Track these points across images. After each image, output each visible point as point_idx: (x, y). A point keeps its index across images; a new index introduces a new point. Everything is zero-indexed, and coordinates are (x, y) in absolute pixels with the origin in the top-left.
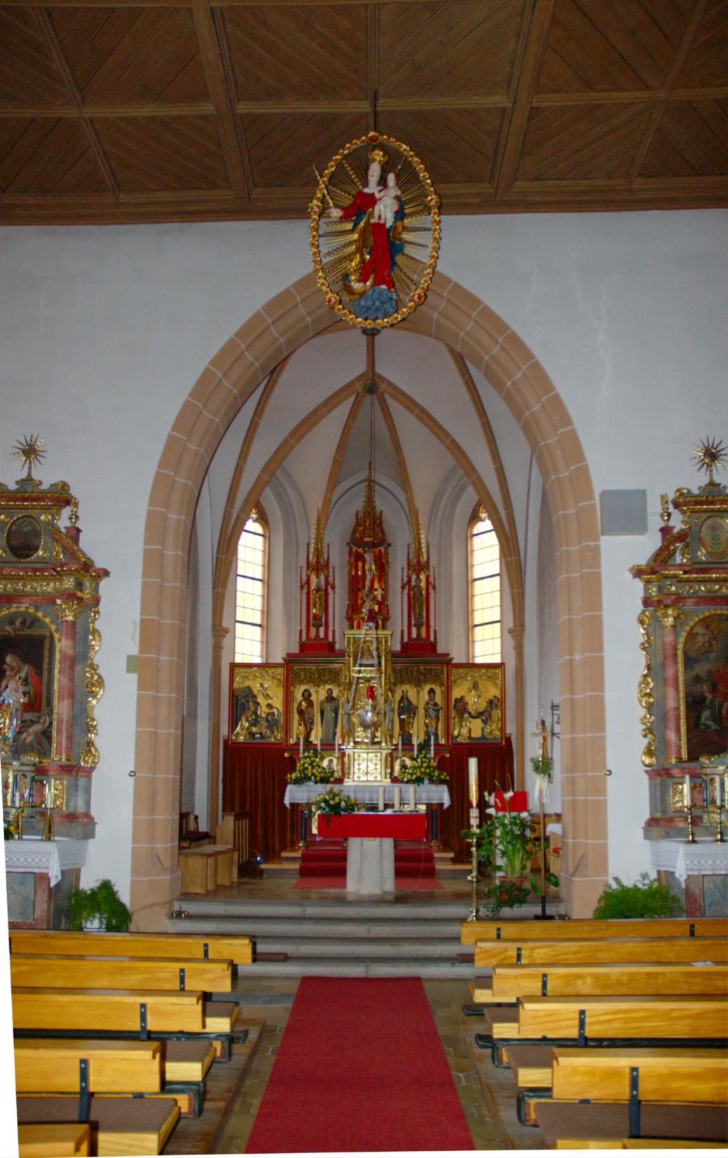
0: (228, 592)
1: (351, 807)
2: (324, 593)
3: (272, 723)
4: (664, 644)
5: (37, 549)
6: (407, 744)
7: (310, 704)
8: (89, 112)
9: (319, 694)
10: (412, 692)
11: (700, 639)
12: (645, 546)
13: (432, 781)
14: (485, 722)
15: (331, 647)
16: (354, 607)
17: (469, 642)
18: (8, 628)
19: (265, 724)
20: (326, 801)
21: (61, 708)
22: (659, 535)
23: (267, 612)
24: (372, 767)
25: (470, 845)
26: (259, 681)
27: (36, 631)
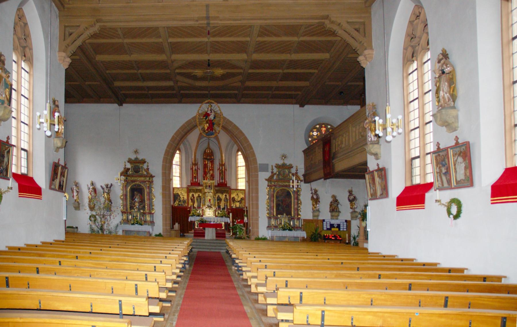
0: (172, 170)
1: (205, 221)
2: (197, 171)
3: (184, 201)
4: (271, 194)
5: (139, 171)
6: (219, 207)
7: (194, 197)
8: (140, 71)
9: (196, 195)
10: (220, 195)
11: (280, 193)
12: (268, 175)
13: (225, 217)
14: (240, 203)
15: (199, 183)
16: (205, 173)
17: (237, 183)
18: (135, 187)
19: (182, 202)
20: (201, 220)
21: (147, 202)
22: (271, 173)
23: (181, 173)
24: (210, 213)
25: (230, 229)
26: (181, 191)
27: (141, 187)
